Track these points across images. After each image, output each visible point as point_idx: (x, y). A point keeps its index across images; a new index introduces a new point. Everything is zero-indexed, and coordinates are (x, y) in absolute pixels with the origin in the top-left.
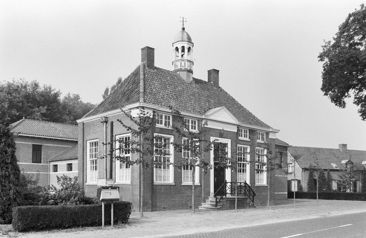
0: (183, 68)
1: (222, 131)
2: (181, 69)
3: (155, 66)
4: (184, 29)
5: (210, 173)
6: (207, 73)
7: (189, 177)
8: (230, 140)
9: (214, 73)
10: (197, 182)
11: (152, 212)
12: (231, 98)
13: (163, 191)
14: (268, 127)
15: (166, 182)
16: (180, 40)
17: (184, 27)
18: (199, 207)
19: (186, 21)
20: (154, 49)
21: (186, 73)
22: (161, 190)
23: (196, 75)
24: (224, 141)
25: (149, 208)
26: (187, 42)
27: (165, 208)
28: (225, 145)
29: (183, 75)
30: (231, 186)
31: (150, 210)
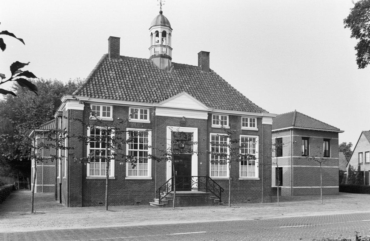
0: (157, 54)
1: (183, 119)
2: (155, 55)
3: (121, 55)
4: (161, 12)
5: (166, 166)
6: (197, 56)
7: (248, 172)
8: (197, 129)
9: (204, 56)
10: (112, 175)
11: (83, 208)
12: (223, 81)
13: (99, 185)
14: (261, 110)
15: (223, 177)
16: (155, 25)
17: (162, 10)
18: (150, 203)
19: (164, 4)
20: (119, 38)
21: (159, 58)
22: (97, 184)
23: (176, 59)
24: (190, 130)
25: (79, 203)
26: (160, 26)
27: (102, 203)
28: (191, 134)
29: (157, 62)
30: (199, 180)
31: (81, 205)
